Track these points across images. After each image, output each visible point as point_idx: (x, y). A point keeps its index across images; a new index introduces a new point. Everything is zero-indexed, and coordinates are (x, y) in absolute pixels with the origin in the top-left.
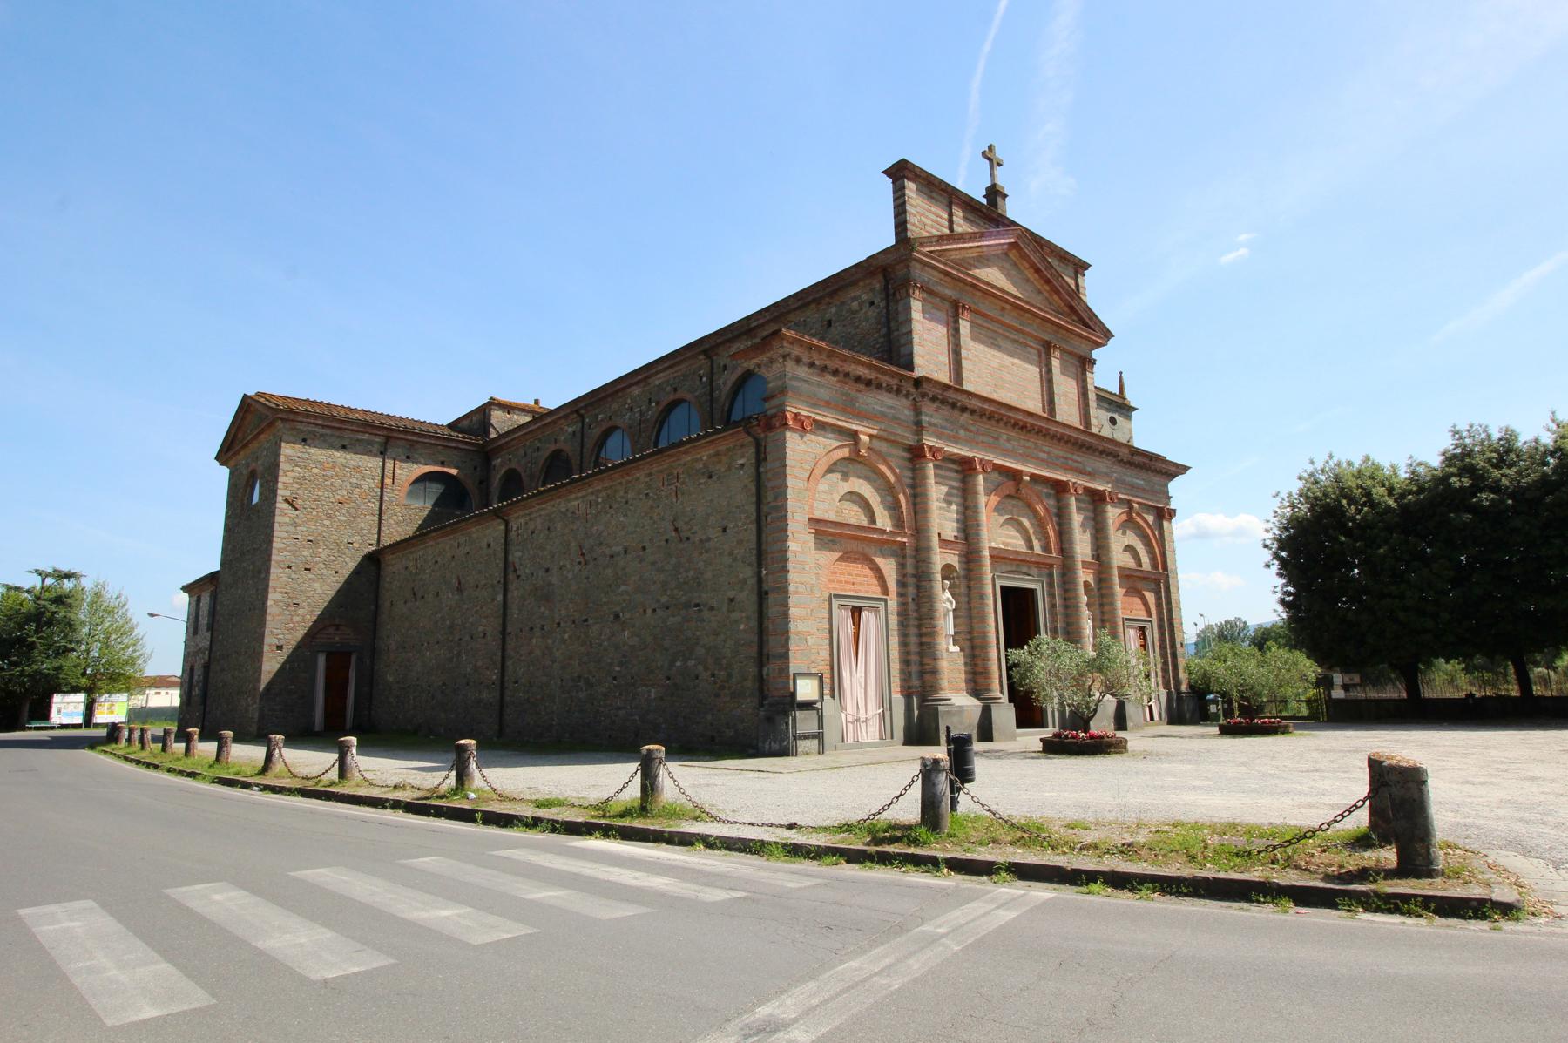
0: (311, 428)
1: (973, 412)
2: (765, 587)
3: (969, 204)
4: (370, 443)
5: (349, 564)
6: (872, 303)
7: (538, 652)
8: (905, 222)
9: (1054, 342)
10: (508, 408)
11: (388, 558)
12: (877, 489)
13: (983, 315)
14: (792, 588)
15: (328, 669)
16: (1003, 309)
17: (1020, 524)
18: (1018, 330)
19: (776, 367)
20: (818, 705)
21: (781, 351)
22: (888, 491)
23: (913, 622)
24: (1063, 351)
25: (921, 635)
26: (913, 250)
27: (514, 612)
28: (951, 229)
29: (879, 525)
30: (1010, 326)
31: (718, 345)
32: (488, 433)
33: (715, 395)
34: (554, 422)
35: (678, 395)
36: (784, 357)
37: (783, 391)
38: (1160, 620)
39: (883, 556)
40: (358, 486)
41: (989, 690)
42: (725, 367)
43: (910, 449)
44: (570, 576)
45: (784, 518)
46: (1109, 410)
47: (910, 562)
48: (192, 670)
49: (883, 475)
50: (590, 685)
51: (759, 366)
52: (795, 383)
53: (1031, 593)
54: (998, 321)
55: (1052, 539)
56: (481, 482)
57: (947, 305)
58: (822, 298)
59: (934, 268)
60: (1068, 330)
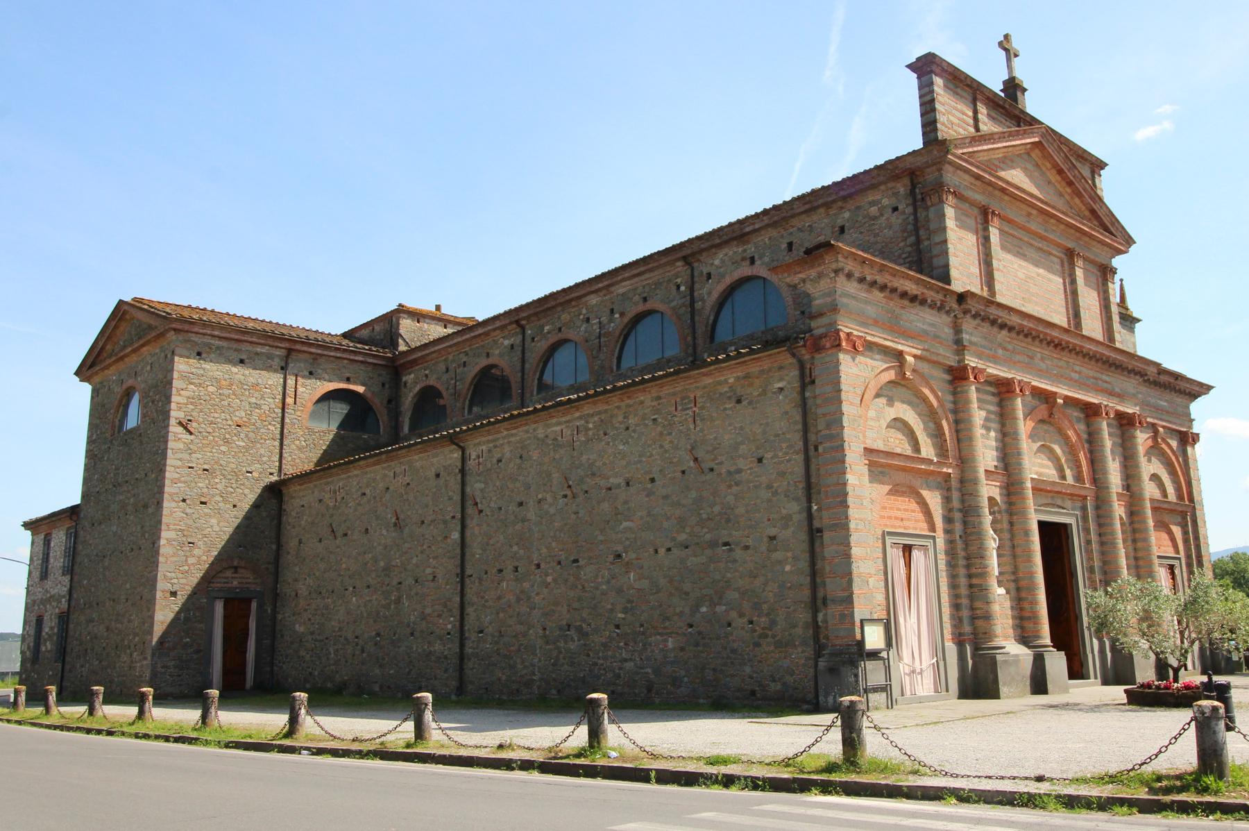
0: (207, 340)
1: (1011, 329)
2: (816, 524)
3: (992, 101)
4: (270, 357)
5: (248, 496)
6: (895, 209)
7: (512, 598)
8: (935, 121)
9: (1077, 250)
10: (418, 316)
11: (293, 489)
12: (919, 415)
13: (1010, 221)
14: (852, 525)
15: (226, 617)
16: (1029, 214)
17: (1052, 451)
19: (824, 284)
20: (884, 654)
21: (834, 266)
22: (931, 416)
23: (962, 562)
24: (1085, 259)
25: (970, 576)
26: (948, 152)
27: (475, 551)
28: (977, 130)
29: (924, 454)
31: (701, 251)
32: (396, 345)
33: (730, 309)
34: (487, 334)
35: (648, 306)
36: (836, 271)
37: (834, 309)
38: (1189, 557)
39: (929, 488)
40: (258, 406)
41: (1038, 637)
42: (709, 276)
43: (950, 370)
44: (552, 511)
45: (841, 448)
47: (955, 495)
48: (40, 621)
49: (925, 400)
50: (583, 634)
51: (804, 281)
52: (845, 300)
53: (1065, 527)
54: (1023, 228)
55: (1085, 468)
56: (389, 401)
57: (976, 211)
58: (834, 201)
59: (967, 171)
60: (1091, 236)
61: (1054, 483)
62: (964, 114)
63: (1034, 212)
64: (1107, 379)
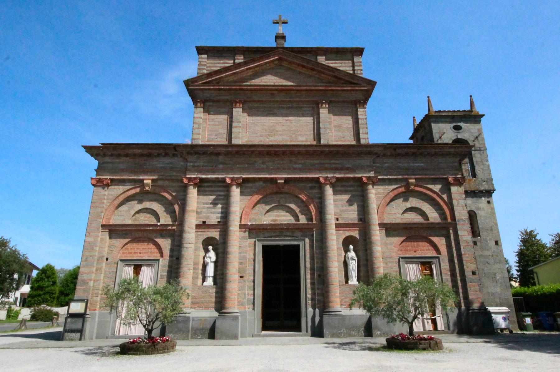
16: (273, 94)
46: (450, 122)
54: (270, 101)
61: (421, 224)
64: (337, 162)
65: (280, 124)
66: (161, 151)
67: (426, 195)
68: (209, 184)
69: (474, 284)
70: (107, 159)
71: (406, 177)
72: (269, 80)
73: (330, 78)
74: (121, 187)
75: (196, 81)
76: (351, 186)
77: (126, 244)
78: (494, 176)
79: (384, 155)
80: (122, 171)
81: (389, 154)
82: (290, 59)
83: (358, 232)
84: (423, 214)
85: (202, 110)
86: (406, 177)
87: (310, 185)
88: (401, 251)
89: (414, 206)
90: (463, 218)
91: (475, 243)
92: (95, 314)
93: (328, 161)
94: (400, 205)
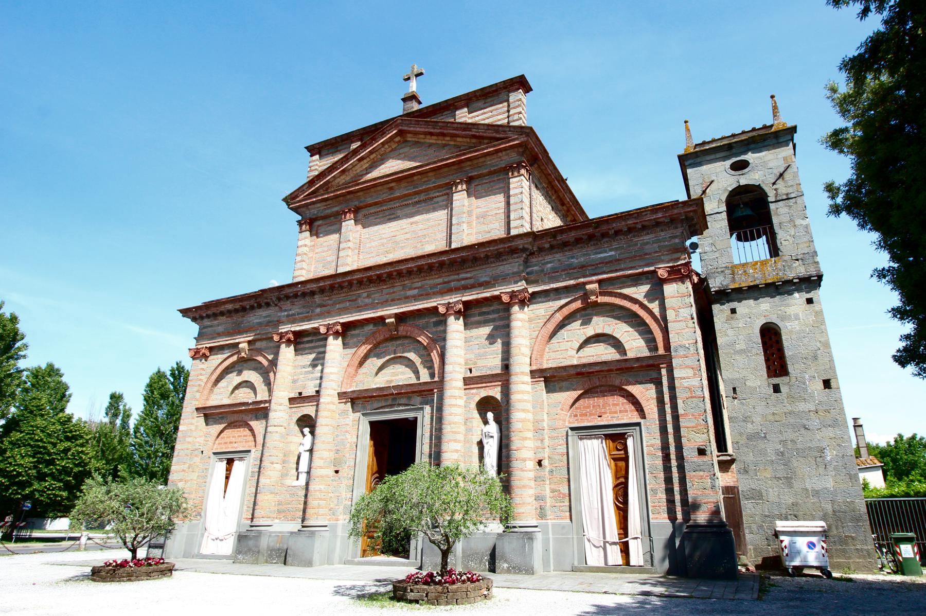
16: (391, 189)
18: (416, 193)
30: (406, 195)
46: (724, 159)
54: (391, 200)
59: (313, 203)
61: (618, 361)
62: (356, 152)
63: (393, 184)
64: (468, 275)
65: (402, 231)
66: (252, 302)
67: (622, 308)
68: (310, 339)
69: (701, 473)
70: (207, 322)
71: (582, 280)
72: (392, 166)
73: (468, 140)
74: (219, 356)
75: (297, 197)
76: (493, 312)
77: (222, 432)
78: (818, 246)
79: (541, 250)
80: (220, 335)
81: (547, 246)
82: (412, 129)
83: (499, 389)
84: (617, 344)
85: (308, 233)
86: (582, 280)
87: (434, 320)
88: (575, 416)
89: (599, 331)
90: (686, 343)
91: (776, 389)
92: (553, 525)
93: (456, 277)
94: (577, 331)
